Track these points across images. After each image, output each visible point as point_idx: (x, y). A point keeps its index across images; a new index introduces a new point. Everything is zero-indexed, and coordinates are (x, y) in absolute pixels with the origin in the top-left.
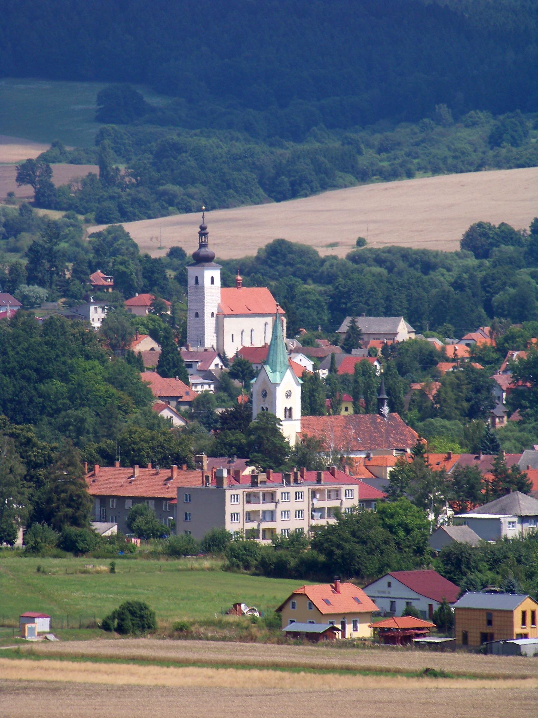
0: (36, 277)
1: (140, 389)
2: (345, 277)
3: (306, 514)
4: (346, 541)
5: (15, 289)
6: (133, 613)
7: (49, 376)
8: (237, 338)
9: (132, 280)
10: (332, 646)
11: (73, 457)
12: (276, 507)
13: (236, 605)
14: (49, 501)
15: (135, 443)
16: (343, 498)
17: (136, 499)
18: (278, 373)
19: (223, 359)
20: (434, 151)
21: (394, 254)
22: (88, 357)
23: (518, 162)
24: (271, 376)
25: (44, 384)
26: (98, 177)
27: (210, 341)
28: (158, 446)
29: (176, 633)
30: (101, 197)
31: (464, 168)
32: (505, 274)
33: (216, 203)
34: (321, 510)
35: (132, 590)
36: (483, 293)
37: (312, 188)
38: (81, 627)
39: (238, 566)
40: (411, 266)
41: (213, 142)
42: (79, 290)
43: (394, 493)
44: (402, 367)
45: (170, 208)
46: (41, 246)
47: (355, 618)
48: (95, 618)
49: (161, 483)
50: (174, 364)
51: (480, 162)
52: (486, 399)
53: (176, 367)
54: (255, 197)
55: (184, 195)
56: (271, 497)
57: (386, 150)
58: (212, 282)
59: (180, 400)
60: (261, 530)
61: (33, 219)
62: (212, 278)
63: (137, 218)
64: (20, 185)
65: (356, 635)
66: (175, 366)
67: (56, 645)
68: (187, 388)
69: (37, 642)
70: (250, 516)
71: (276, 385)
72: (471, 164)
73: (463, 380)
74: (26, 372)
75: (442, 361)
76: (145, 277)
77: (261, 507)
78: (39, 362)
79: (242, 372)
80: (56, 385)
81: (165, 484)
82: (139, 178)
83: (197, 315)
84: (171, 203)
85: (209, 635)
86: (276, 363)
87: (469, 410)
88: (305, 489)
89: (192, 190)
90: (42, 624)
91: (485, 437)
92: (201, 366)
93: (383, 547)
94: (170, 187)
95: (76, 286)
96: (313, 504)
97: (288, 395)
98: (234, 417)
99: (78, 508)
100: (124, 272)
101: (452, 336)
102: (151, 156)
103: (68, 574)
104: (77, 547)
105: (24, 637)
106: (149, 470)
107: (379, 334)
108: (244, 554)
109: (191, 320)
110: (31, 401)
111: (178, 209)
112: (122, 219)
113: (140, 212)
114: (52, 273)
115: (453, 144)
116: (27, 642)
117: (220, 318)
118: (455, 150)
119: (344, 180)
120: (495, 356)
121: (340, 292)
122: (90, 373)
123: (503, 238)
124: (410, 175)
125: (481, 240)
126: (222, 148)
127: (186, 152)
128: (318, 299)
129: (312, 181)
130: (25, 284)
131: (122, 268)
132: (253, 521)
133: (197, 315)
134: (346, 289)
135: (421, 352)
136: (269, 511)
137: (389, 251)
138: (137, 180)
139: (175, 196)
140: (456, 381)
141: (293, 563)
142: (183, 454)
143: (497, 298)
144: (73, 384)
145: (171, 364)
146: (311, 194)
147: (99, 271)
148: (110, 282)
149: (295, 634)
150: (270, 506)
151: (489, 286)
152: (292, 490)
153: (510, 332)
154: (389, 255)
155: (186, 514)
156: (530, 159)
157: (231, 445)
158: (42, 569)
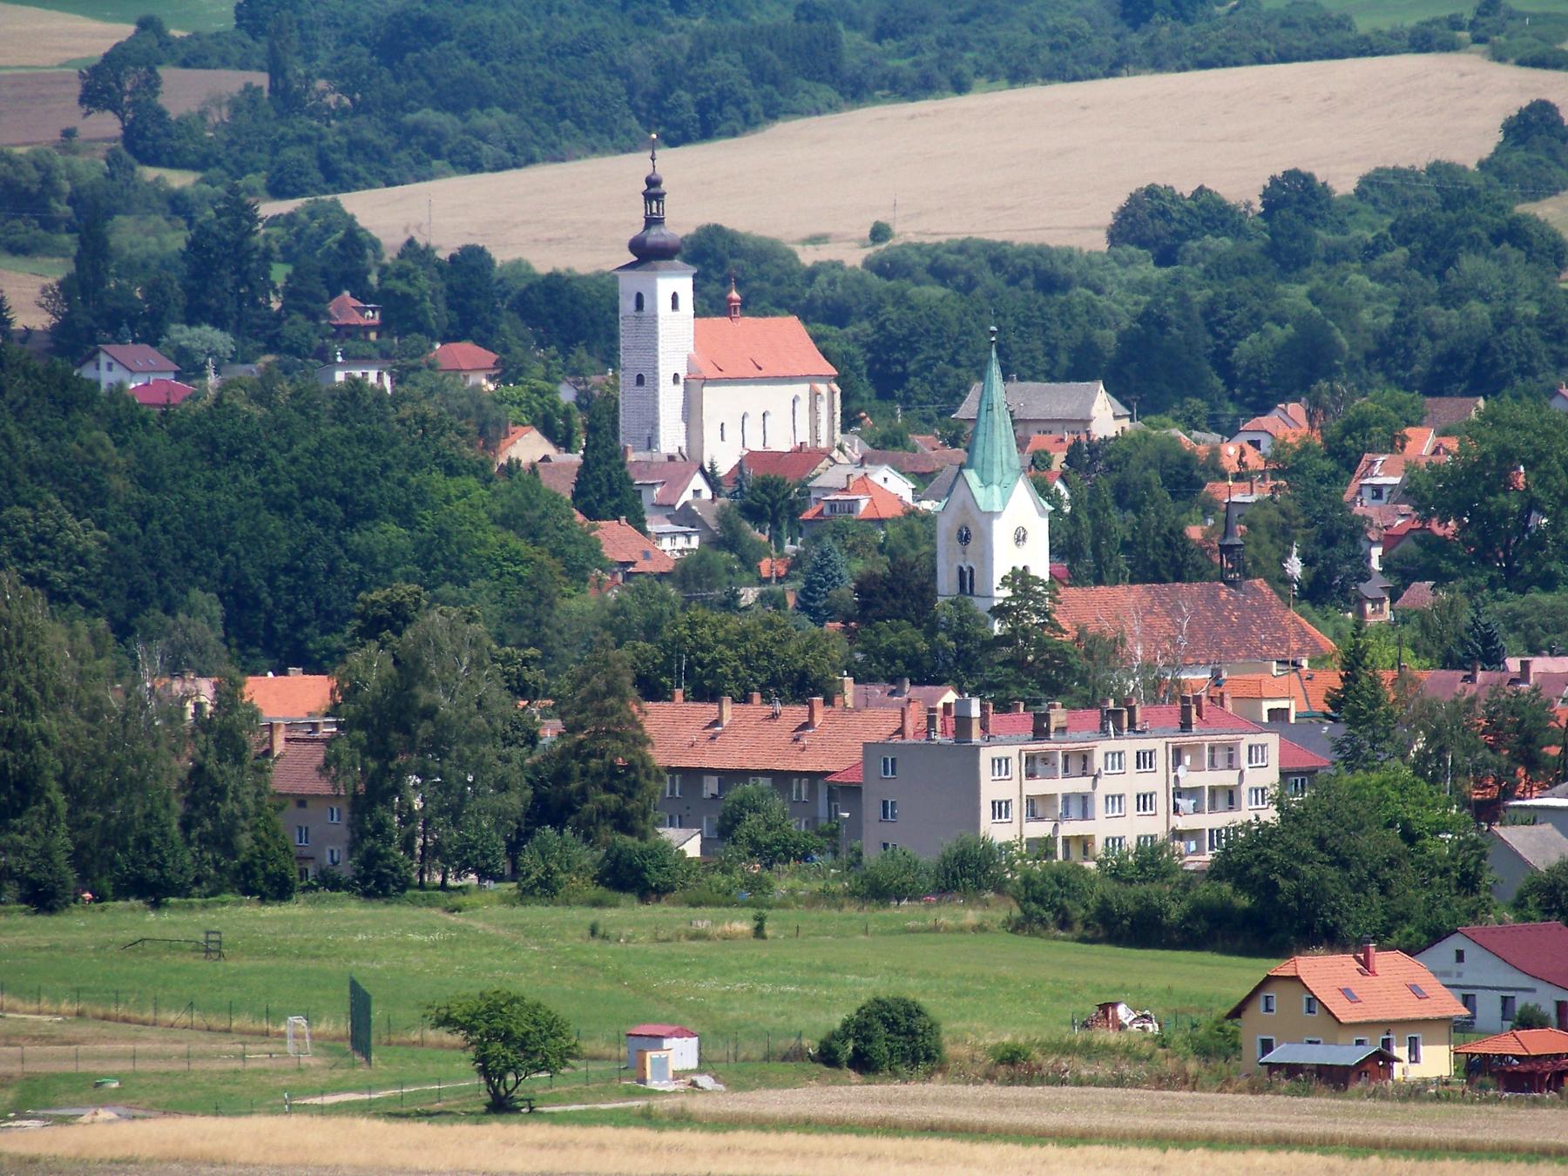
0: (208, 308)
1: (575, 542)
2: (897, 303)
3: (1161, 802)
4: (1304, 859)
5: (159, 335)
6: (892, 1025)
7: (370, 514)
8: (733, 433)
9: (424, 312)
10: (1385, 1097)
11: (617, 675)
12: (1094, 787)
13: (1106, 1008)
14: (562, 776)
15: (703, 649)
16: (1244, 763)
17: (729, 777)
18: (995, 488)
19: (711, 478)
20: (999, 33)
21: (972, 257)
22: (451, 470)
23: (1201, 57)
24: (979, 493)
25: (359, 531)
26: (266, 94)
27: (671, 437)
28: (760, 653)
29: (1002, 1069)
30: (282, 138)
31: (1081, 73)
32: (1256, 294)
33: (536, 150)
34: (1194, 792)
35: (821, 976)
36: (1209, 339)
37: (746, 116)
38: (767, 1058)
39: (1042, 921)
40: (1013, 281)
41: (511, 17)
42: (306, 335)
43: (1356, 751)
44: (1125, 493)
45: (435, 162)
46: (215, 236)
47: (1416, 1031)
48: (800, 1036)
49: (787, 737)
50: (611, 488)
51: (1115, 57)
52: (1349, 558)
53: (618, 495)
54: (622, 137)
55: (464, 132)
56: (1081, 762)
57: (893, 33)
58: (675, 306)
59: (631, 569)
60: (1060, 841)
61: (136, 187)
62: (675, 297)
63: (361, 184)
64: (88, 113)
65: (1416, 1072)
66: (613, 494)
67: (715, 1097)
68: (645, 544)
69: (675, 1093)
70: (1035, 808)
71: (992, 515)
72: (1097, 61)
73: (1296, 518)
74: (317, 503)
75: (1213, 480)
76: (450, 306)
77: (1060, 786)
78: (347, 480)
79: (772, 506)
80: (388, 534)
81: (796, 740)
82: (358, 96)
83: (640, 380)
84: (434, 151)
85: (1084, 1073)
86: (992, 463)
87: (1310, 584)
88: (1159, 746)
89: (480, 120)
90: (681, 1053)
91: (1468, 630)
92: (663, 494)
93: (1387, 873)
94: (429, 116)
95: (297, 327)
96: (1177, 778)
97: (1020, 537)
98: (891, 590)
99: (630, 795)
100: (406, 297)
101: (1203, 424)
102: (364, 50)
103: (658, 941)
104: (645, 880)
105: (643, 1080)
106: (758, 707)
107: (1052, 421)
108: (1055, 894)
109: (627, 396)
110: (332, 570)
111: (453, 163)
112: (329, 187)
113: (369, 170)
114: (241, 298)
115: (1043, 20)
116: (653, 1093)
117: (693, 386)
118: (1054, 31)
119: (814, 98)
120: (1328, 465)
121: (890, 336)
122: (459, 506)
123: (1204, 220)
124: (960, 87)
125: (1156, 223)
126: (529, 29)
127: (450, 38)
128: (846, 353)
129: (746, 101)
130: (182, 322)
131: (401, 286)
132: (1041, 819)
133: (640, 380)
134: (905, 331)
135: (1163, 460)
136: (1225, 787)
137: (962, 248)
138: (353, 100)
139: (441, 135)
140: (1279, 519)
141: (1175, 912)
142: (816, 673)
143: (1245, 349)
144: (422, 530)
145: (605, 490)
146: (744, 130)
147: (347, 293)
148: (372, 317)
149: (1292, 1070)
150: (1082, 785)
151: (1220, 322)
152: (1130, 746)
153: (1357, 413)
154: (962, 258)
155: (885, 803)
156: (1228, 50)
157: (891, 655)
158: (601, 931)
